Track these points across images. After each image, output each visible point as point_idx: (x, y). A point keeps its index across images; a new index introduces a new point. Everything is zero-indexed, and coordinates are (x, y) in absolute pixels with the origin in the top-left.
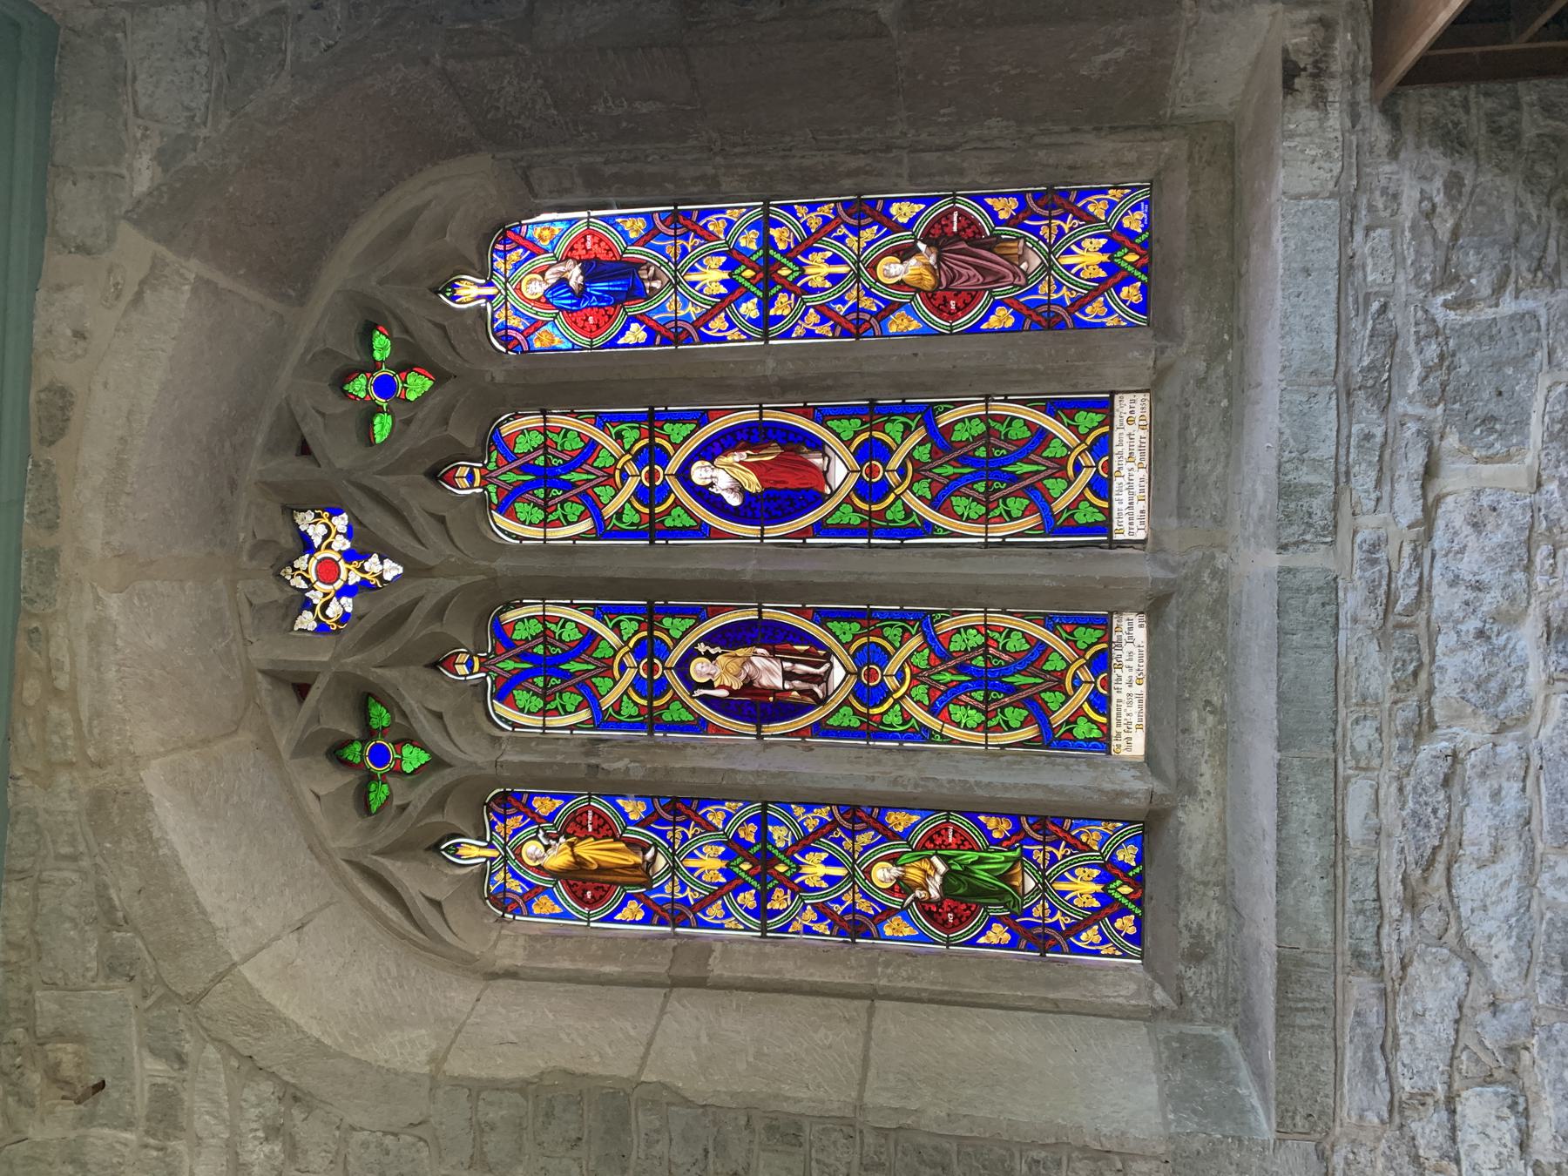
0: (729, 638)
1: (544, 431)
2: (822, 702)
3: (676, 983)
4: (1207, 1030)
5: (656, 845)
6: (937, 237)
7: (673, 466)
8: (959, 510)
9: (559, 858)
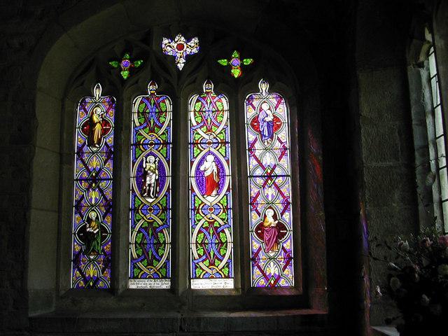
0: (160, 167)
1: (223, 110)
2: (142, 195)
3: (61, 154)
4: (54, 305)
5: (100, 147)
6: (280, 226)
7: (212, 150)
8: (199, 235)
9: (96, 119)
